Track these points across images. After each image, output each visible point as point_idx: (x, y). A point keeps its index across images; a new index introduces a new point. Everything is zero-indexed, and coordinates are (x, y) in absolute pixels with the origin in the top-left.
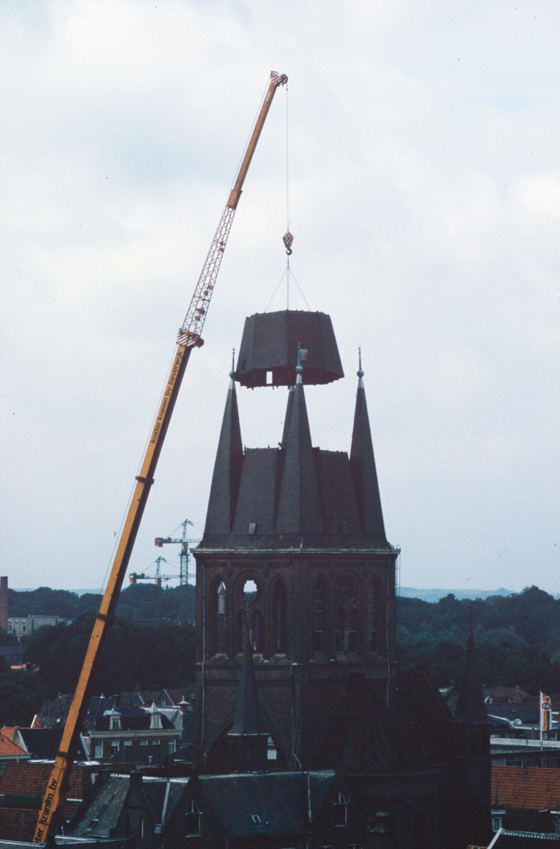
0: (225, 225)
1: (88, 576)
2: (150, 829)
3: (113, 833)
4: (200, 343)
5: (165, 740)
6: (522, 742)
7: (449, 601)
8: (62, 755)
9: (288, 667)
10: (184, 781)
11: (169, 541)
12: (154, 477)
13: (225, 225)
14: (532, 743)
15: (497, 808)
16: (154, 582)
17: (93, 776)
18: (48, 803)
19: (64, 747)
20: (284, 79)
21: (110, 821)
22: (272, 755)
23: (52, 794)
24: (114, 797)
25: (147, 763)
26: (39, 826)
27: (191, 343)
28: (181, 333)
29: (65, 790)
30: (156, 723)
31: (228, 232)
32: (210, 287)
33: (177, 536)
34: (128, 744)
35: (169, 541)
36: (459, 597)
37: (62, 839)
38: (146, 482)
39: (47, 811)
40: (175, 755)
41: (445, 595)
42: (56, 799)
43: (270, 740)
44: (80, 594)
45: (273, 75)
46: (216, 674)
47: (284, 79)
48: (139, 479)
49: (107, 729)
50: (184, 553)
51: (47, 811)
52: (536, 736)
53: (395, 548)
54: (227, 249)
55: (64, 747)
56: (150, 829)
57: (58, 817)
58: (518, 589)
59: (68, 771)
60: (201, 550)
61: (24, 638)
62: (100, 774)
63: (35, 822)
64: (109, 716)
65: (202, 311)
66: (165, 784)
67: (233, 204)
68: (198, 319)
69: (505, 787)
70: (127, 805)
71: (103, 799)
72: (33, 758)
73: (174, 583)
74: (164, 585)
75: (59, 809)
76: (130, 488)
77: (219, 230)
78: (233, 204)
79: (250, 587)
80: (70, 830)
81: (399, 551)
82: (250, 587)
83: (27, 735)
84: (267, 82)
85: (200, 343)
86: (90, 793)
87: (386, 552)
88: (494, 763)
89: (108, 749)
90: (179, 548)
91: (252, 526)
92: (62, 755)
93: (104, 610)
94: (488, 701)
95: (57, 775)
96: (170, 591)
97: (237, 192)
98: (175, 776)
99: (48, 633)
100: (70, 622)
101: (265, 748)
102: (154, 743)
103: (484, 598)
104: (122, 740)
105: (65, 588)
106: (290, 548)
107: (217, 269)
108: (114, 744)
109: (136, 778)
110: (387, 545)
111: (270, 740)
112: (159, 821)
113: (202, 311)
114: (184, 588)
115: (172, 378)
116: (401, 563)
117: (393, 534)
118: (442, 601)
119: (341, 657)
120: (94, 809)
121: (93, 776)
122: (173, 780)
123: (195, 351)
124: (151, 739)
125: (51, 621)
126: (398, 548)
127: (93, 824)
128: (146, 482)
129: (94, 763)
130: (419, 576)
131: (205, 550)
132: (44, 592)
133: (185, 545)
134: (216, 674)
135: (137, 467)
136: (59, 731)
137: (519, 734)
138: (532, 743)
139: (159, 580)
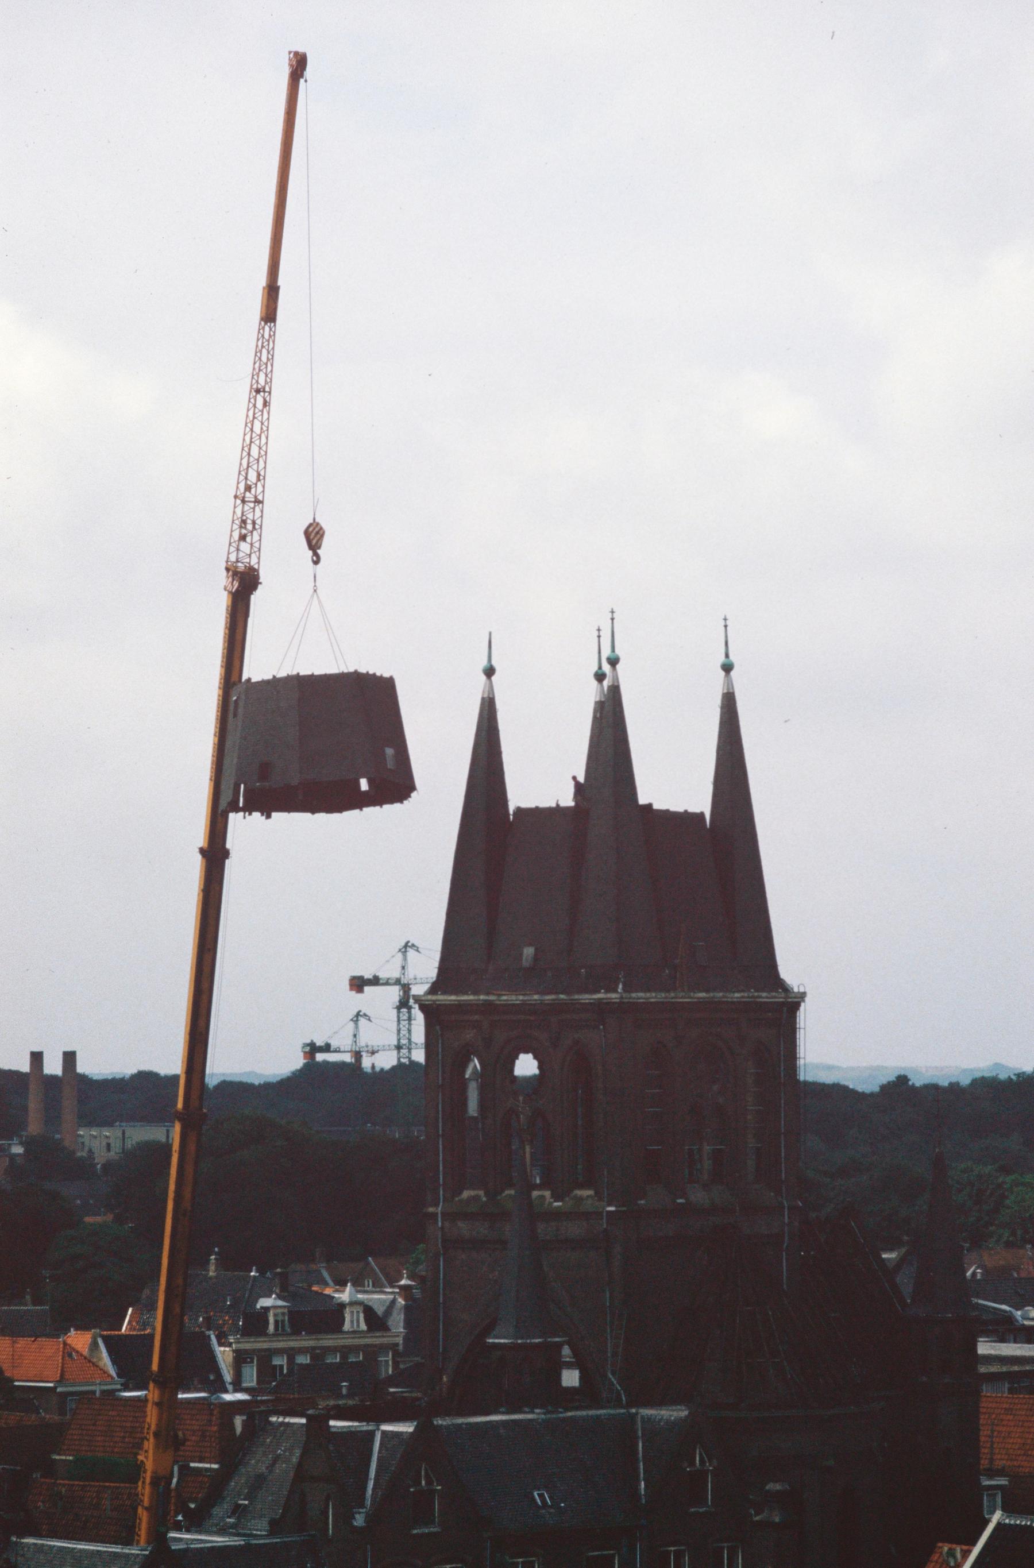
2: (345, 1518)
3: (275, 1527)
5: (372, 1353)
7: (899, 1088)
9: (599, 1214)
10: (406, 1428)
11: (375, 981)
15: (992, 1473)
16: (348, 1058)
17: (238, 1421)
22: (571, 1378)
24: (277, 1460)
30: (353, 1321)
34: (303, 1360)
35: (375, 981)
37: (182, 1538)
40: (391, 1381)
41: (892, 1078)
43: (566, 1351)
46: (464, 1228)
50: (403, 1004)
53: (796, 990)
56: (345, 1518)
60: (434, 998)
61: (107, 1166)
64: (266, 1309)
66: (371, 1434)
67: (269, 315)
70: (300, 1474)
71: (257, 1463)
73: (386, 1061)
74: (367, 1063)
78: (269, 315)
80: (196, 1521)
81: (802, 996)
82: (526, 1066)
87: (779, 997)
90: (394, 994)
91: (529, 952)
97: (272, 291)
102: (352, 1359)
104: (291, 1354)
106: (599, 992)
108: (277, 1361)
109: (317, 1424)
110: (779, 984)
111: (566, 1351)
116: (807, 1018)
117: (791, 968)
119: (698, 1196)
120: (238, 1483)
121: (238, 1421)
122: (386, 1427)
124: (345, 1351)
126: (802, 990)
127: (237, 1510)
129: (240, 1396)
130: (840, 1043)
131: (441, 998)
134: (464, 1228)
139: (358, 1055)
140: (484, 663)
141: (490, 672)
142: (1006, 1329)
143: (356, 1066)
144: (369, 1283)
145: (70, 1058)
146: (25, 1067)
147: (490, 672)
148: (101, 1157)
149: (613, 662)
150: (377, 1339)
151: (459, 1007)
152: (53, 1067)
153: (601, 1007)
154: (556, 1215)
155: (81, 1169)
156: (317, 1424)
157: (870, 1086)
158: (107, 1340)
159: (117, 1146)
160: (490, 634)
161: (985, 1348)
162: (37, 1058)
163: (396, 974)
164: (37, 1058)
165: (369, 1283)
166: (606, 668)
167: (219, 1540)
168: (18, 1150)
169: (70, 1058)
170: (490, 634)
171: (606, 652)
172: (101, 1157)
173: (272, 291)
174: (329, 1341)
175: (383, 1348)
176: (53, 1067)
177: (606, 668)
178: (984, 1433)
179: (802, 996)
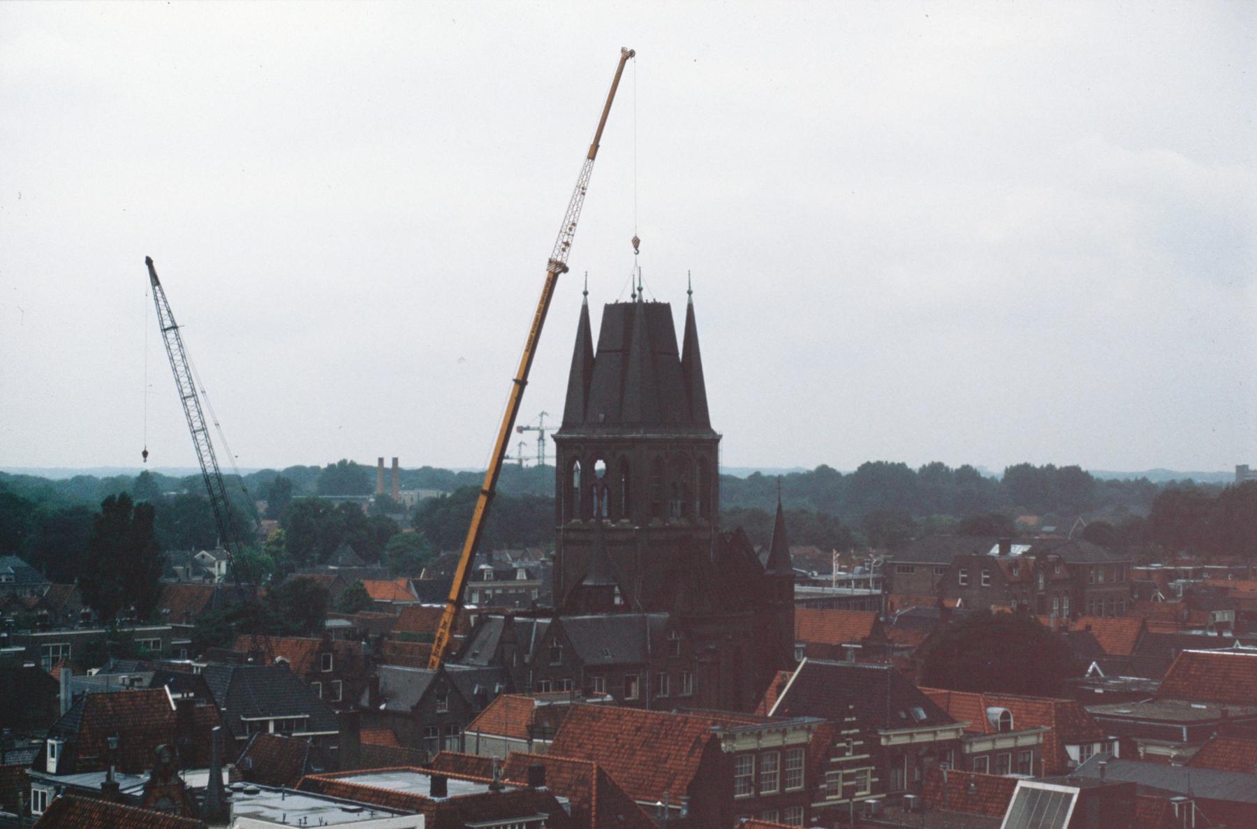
0: (586, 173)
1: (473, 457)
2: (521, 658)
3: (491, 663)
4: (565, 270)
5: (529, 589)
6: (818, 589)
7: (756, 477)
8: (451, 602)
9: (631, 530)
10: (548, 621)
11: (528, 428)
12: (529, 379)
13: (586, 173)
14: (828, 590)
15: (801, 642)
16: (516, 462)
17: (472, 618)
18: (440, 640)
19: (453, 595)
20: (632, 54)
21: (489, 652)
22: (617, 601)
23: (444, 634)
24: (492, 633)
25: (515, 606)
26: (433, 658)
27: (558, 270)
28: (551, 262)
29: (453, 629)
30: (521, 575)
31: (588, 179)
32: (574, 224)
33: (536, 424)
34: (499, 592)
35: (528, 428)
36: (765, 474)
37: (449, 666)
38: (521, 383)
39: (439, 646)
40: (537, 601)
41: (752, 473)
42: (446, 636)
43: (617, 589)
44: (456, 472)
45: (623, 50)
46: (572, 535)
47: (632, 54)
48: (516, 381)
49: (481, 579)
50: (541, 438)
51: (439, 646)
52: (829, 584)
54: (587, 192)
55: (453, 595)
56: (521, 658)
57: (448, 649)
58: (812, 467)
59: (456, 615)
61: (411, 508)
62: (480, 615)
63: (429, 655)
64: (483, 570)
65: (567, 244)
66: (532, 624)
67: (592, 155)
68: (564, 250)
69: (807, 626)
70: (502, 641)
71: (483, 635)
72: (423, 602)
73: (533, 463)
74: (524, 464)
75: (448, 644)
76: (509, 388)
77: (581, 176)
78: (592, 155)
79: (600, 465)
80: (457, 660)
81: (721, 436)
82: (600, 465)
83: (418, 585)
84: (619, 56)
85: (565, 270)
86: (472, 634)
87: (711, 437)
88: (797, 606)
89: (483, 596)
90: (537, 434)
91: (602, 416)
92: (451, 602)
93: (486, 487)
94: (986, 581)
95: (447, 618)
96: (530, 470)
97: (595, 147)
98: (540, 617)
99: (434, 504)
100: (449, 495)
101: (613, 595)
102: (520, 592)
103: (785, 474)
104: (494, 589)
105: (444, 467)
107: (579, 209)
108: (488, 592)
109: (509, 618)
111: (617, 589)
112: (528, 652)
113: (567, 244)
114: (542, 467)
115: (543, 298)
116: (722, 445)
117: (716, 424)
118: (751, 477)
119: (674, 521)
120: (476, 643)
121: (472, 618)
122: (539, 621)
123: (562, 276)
124: (517, 588)
125: (434, 493)
127: (475, 655)
128: (521, 383)
129: (473, 607)
130: (734, 459)
132: (426, 470)
133: (542, 432)
134: (572, 535)
135: (514, 371)
136: (449, 582)
137: (816, 583)
138: (828, 590)
139: (521, 461)
140: (583, 289)
141: (586, 293)
142: (806, 581)
143: (520, 466)
144: (526, 560)
145: (395, 461)
146: (376, 464)
147: (586, 293)
148: (409, 503)
149: (640, 289)
150: (531, 583)
151: (571, 440)
152: (388, 464)
153: (633, 440)
154: (612, 530)
155: (399, 508)
156: (509, 618)
157: (744, 476)
158: (414, 582)
159: (415, 499)
160: (149, 262)
161: (797, 588)
162: (381, 460)
163: (537, 425)
164: (381, 460)
165: (526, 560)
166: (637, 292)
167: (467, 668)
168: (372, 500)
169: (395, 461)
170: (149, 262)
171: (637, 285)
172: (409, 503)
173: (595, 147)
174: (510, 584)
175: (534, 588)
176: (388, 464)
177: (637, 292)
178: (796, 625)
179: (721, 436)
